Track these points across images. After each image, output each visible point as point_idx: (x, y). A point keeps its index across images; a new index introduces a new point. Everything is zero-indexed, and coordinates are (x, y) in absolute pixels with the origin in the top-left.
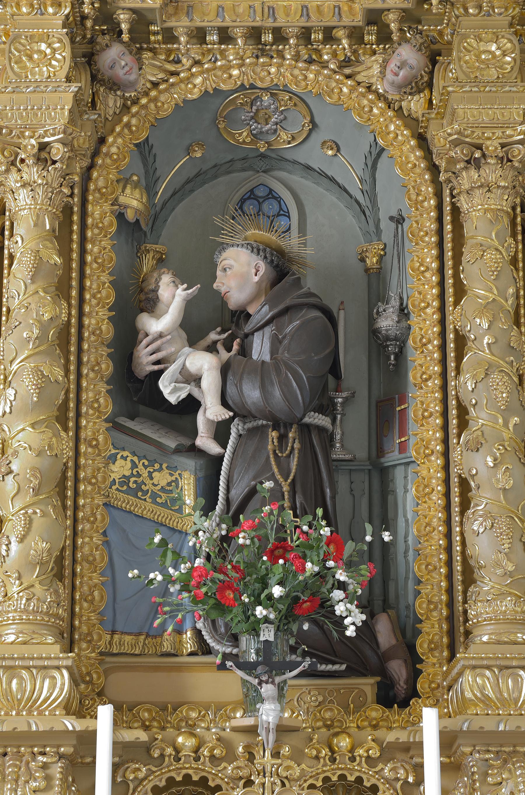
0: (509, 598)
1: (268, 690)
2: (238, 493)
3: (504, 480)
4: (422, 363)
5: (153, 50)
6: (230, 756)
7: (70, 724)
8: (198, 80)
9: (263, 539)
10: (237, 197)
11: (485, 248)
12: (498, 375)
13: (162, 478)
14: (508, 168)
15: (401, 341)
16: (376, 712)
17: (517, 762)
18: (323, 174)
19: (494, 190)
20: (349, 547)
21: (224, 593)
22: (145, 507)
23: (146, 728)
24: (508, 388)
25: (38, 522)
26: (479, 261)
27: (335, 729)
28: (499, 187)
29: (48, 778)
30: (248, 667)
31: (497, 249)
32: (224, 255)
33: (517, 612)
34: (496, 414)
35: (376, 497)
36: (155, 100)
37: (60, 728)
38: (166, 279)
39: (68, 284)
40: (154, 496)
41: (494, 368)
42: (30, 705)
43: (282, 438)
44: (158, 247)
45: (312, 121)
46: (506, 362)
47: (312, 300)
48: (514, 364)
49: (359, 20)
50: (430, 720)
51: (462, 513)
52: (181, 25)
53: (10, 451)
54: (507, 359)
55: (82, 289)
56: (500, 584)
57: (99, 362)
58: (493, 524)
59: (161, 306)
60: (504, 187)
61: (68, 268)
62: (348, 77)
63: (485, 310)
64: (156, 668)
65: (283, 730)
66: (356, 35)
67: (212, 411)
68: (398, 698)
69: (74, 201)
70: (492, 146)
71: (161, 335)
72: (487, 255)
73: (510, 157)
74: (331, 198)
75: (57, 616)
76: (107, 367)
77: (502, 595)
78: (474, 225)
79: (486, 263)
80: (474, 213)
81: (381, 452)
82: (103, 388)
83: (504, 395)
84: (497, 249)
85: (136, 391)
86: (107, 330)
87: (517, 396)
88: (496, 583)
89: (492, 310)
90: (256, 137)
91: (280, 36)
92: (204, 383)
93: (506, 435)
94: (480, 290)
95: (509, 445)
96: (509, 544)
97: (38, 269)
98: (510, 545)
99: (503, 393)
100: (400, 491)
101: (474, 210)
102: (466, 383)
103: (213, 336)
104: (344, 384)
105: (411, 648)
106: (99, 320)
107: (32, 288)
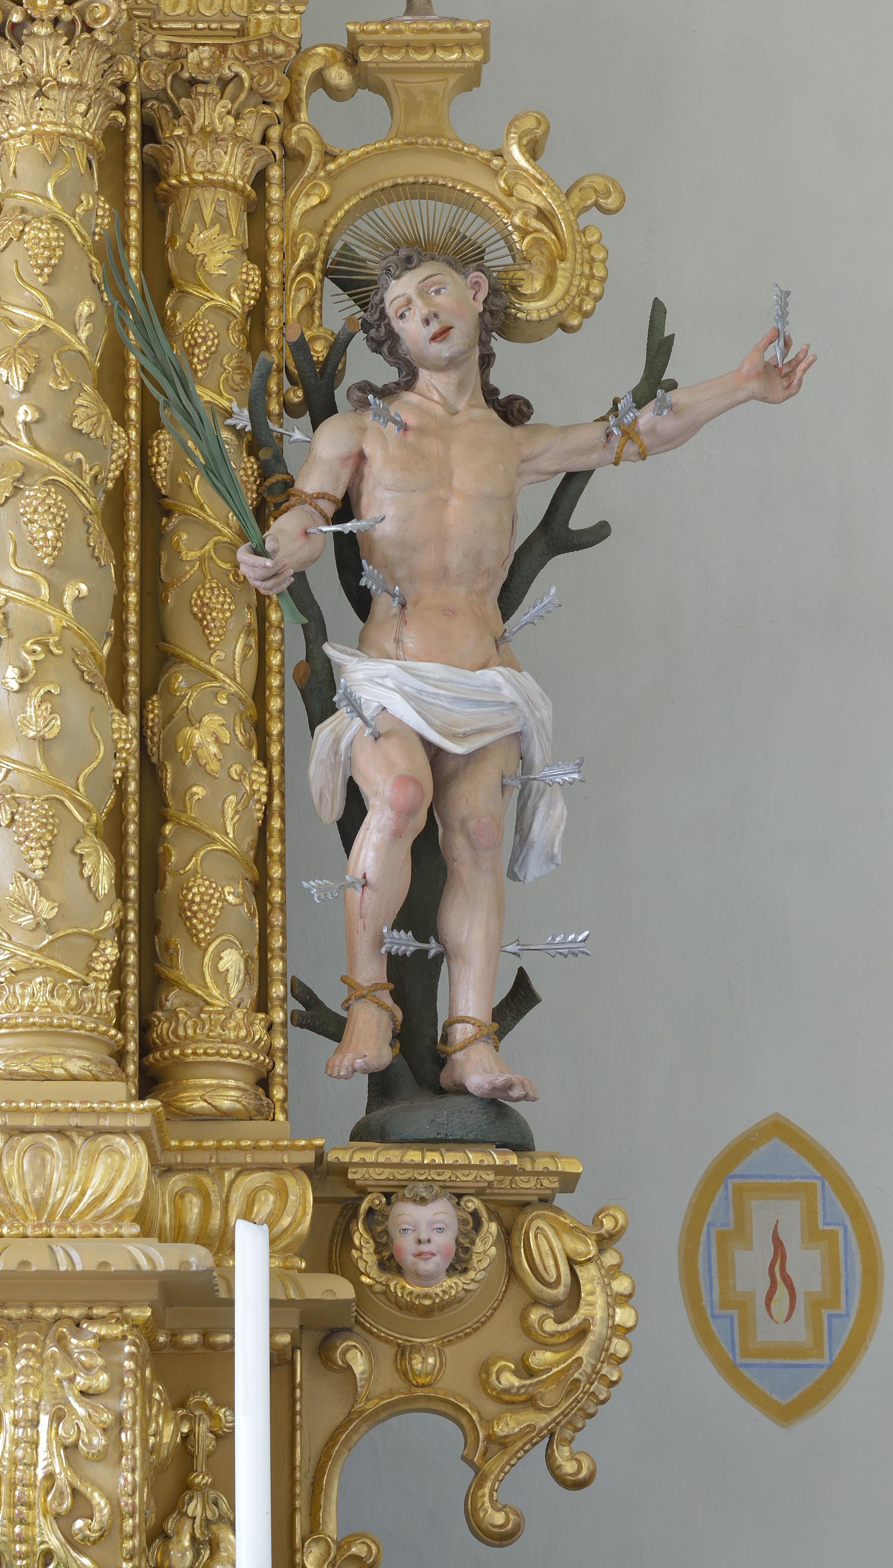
0: (39, 979)
3: (41, 720)
11: (27, 217)
12: (39, 490)
14: (85, 45)
17: (24, 1340)
19: (52, 93)
24: (59, 520)
26: (14, 244)
28: (61, 85)
31: (55, 220)
33: (55, 1009)
34: (36, 576)
37: (125, 1265)
41: (37, 476)
46: (67, 465)
48: (86, 467)
54: (68, 456)
56: (26, 948)
58: (13, 814)
60: (72, 86)
63: (20, 351)
69: (127, 118)
72: (29, 232)
73: (88, 20)
78: (12, 169)
79: (28, 250)
80: (12, 142)
83: (50, 534)
84: (55, 220)
87: (84, 536)
88: (21, 946)
89: (36, 350)
93: (55, 620)
95: (58, 644)
96: (43, 859)
98: (45, 863)
99: (45, 529)
101: (12, 136)
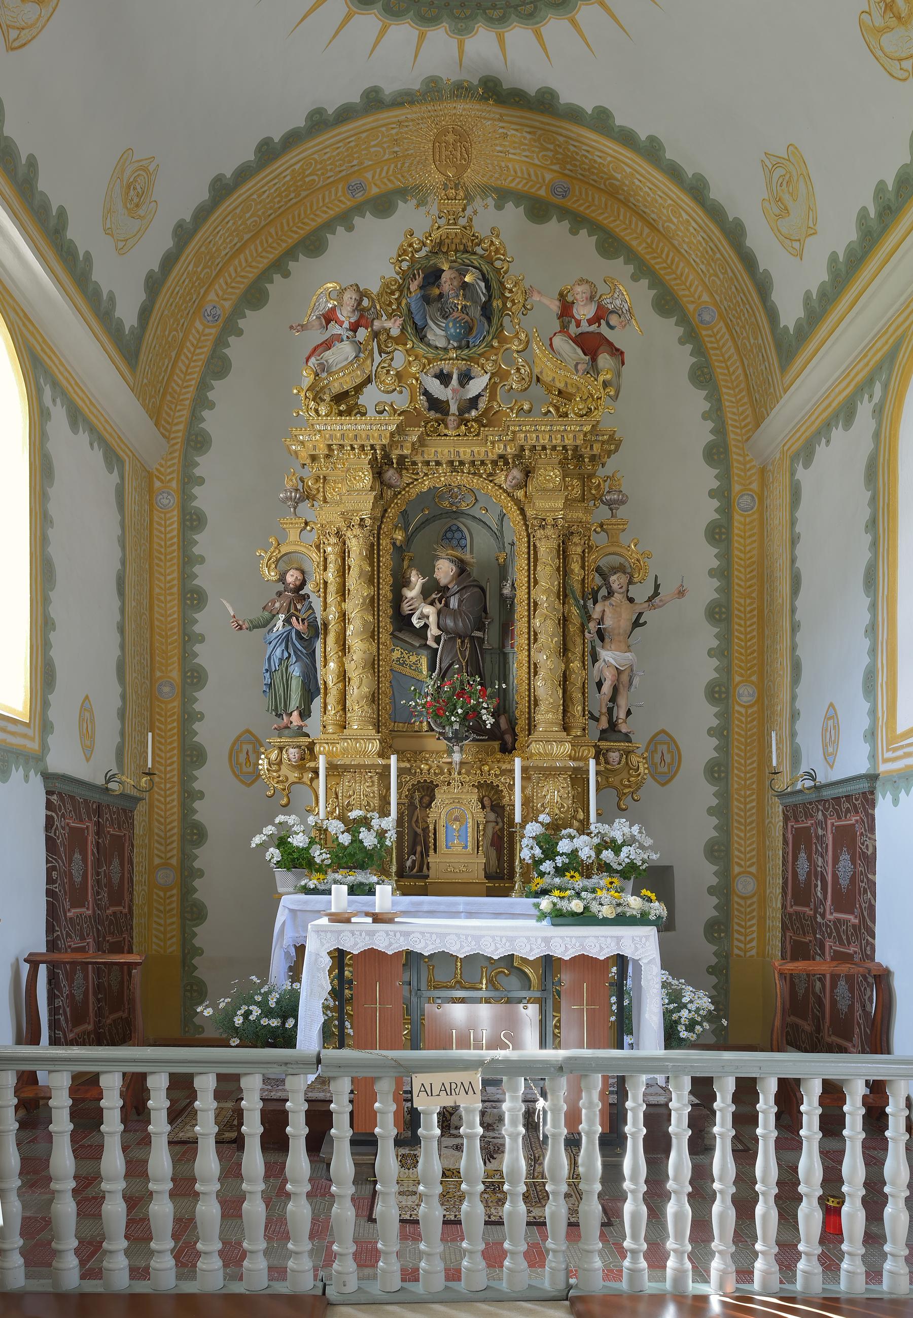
1: (456, 748)
2: (445, 665)
4: (521, 610)
5: (407, 469)
6: (442, 773)
7: (380, 761)
8: (426, 483)
9: (455, 688)
10: (444, 530)
13: (413, 659)
15: (513, 598)
16: (499, 755)
18: (480, 520)
20: (489, 690)
21: (440, 710)
22: (407, 671)
23: (409, 761)
25: (365, 680)
27: (482, 762)
29: (372, 782)
30: (448, 739)
32: (439, 562)
35: (502, 665)
36: (408, 492)
38: (414, 573)
39: (372, 579)
40: (410, 666)
42: (365, 753)
43: (463, 642)
44: (410, 554)
45: (476, 499)
47: (475, 583)
49: (495, 457)
50: (518, 763)
51: (534, 676)
52: (418, 459)
53: (352, 651)
55: (379, 578)
57: (386, 609)
59: (412, 585)
61: (373, 570)
62: (491, 481)
64: (412, 737)
65: (462, 763)
66: (494, 463)
67: (433, 631)
68: (508, 749)
70: (550, 520)
71: (412, 598)
74: (484, 531)
75: (373, 718)
76: (390, 612)
77: (547, 712)
81: (504, 646)
82: (388, 620)
85: (402, 621)
86: (390, 596)
90: (452, 504)
91: (462, 463)
92: (431, 619)
94: (543, 583)
97: (361, 573)
100: (511, 664)
102: (537, 622)
103: (434, 596)
104: (489, 615)
105: (514, 729)
106: (386, 591)
107: (359, 582)
